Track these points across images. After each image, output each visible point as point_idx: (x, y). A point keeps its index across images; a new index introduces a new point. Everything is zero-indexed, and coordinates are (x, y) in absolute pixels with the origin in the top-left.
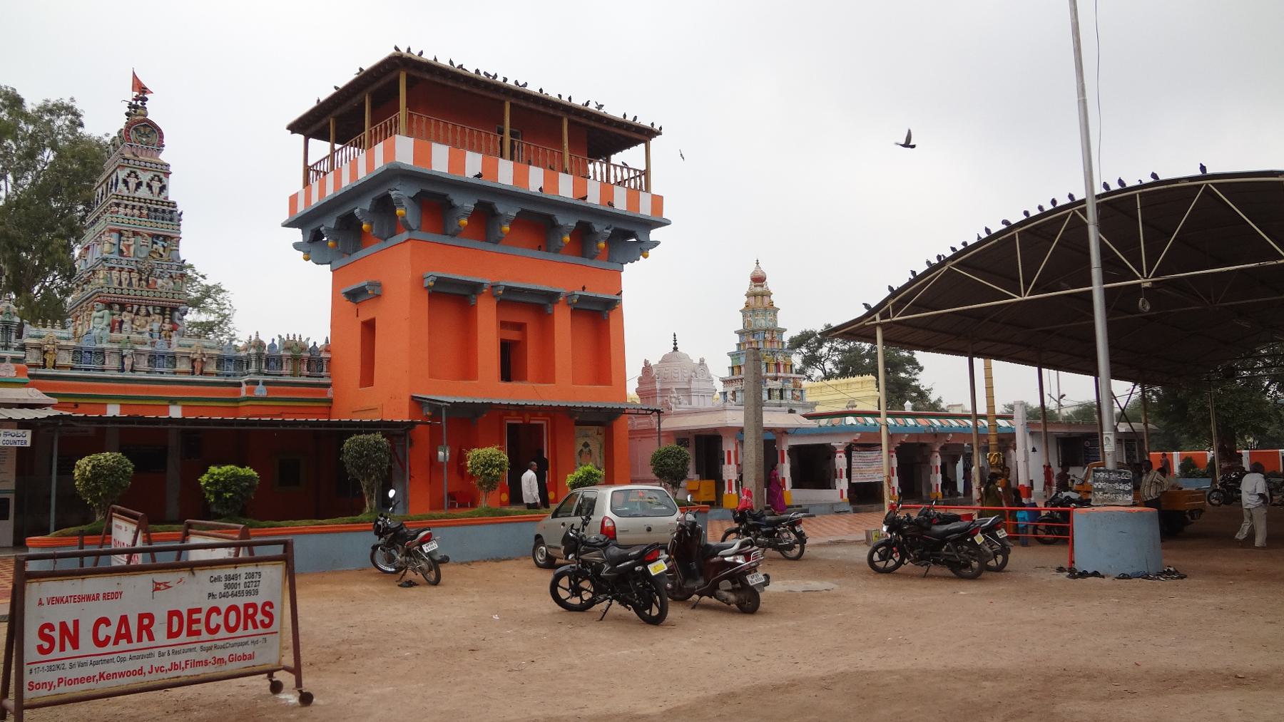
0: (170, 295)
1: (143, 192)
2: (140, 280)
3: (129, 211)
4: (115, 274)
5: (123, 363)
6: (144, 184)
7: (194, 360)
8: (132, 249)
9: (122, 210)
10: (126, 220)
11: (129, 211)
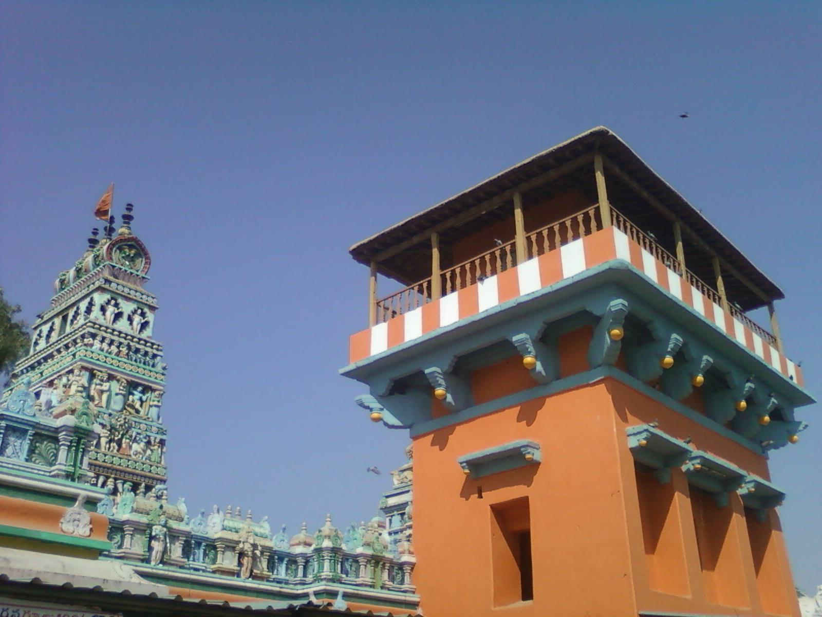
1: (122, 325)
2: (110, 441)
3: (105, 346)
5: (150, 549)
6: (125, 316)
7: (242, 555)
8: (105, 396)
9: (97, 344)
11: (105, 346)
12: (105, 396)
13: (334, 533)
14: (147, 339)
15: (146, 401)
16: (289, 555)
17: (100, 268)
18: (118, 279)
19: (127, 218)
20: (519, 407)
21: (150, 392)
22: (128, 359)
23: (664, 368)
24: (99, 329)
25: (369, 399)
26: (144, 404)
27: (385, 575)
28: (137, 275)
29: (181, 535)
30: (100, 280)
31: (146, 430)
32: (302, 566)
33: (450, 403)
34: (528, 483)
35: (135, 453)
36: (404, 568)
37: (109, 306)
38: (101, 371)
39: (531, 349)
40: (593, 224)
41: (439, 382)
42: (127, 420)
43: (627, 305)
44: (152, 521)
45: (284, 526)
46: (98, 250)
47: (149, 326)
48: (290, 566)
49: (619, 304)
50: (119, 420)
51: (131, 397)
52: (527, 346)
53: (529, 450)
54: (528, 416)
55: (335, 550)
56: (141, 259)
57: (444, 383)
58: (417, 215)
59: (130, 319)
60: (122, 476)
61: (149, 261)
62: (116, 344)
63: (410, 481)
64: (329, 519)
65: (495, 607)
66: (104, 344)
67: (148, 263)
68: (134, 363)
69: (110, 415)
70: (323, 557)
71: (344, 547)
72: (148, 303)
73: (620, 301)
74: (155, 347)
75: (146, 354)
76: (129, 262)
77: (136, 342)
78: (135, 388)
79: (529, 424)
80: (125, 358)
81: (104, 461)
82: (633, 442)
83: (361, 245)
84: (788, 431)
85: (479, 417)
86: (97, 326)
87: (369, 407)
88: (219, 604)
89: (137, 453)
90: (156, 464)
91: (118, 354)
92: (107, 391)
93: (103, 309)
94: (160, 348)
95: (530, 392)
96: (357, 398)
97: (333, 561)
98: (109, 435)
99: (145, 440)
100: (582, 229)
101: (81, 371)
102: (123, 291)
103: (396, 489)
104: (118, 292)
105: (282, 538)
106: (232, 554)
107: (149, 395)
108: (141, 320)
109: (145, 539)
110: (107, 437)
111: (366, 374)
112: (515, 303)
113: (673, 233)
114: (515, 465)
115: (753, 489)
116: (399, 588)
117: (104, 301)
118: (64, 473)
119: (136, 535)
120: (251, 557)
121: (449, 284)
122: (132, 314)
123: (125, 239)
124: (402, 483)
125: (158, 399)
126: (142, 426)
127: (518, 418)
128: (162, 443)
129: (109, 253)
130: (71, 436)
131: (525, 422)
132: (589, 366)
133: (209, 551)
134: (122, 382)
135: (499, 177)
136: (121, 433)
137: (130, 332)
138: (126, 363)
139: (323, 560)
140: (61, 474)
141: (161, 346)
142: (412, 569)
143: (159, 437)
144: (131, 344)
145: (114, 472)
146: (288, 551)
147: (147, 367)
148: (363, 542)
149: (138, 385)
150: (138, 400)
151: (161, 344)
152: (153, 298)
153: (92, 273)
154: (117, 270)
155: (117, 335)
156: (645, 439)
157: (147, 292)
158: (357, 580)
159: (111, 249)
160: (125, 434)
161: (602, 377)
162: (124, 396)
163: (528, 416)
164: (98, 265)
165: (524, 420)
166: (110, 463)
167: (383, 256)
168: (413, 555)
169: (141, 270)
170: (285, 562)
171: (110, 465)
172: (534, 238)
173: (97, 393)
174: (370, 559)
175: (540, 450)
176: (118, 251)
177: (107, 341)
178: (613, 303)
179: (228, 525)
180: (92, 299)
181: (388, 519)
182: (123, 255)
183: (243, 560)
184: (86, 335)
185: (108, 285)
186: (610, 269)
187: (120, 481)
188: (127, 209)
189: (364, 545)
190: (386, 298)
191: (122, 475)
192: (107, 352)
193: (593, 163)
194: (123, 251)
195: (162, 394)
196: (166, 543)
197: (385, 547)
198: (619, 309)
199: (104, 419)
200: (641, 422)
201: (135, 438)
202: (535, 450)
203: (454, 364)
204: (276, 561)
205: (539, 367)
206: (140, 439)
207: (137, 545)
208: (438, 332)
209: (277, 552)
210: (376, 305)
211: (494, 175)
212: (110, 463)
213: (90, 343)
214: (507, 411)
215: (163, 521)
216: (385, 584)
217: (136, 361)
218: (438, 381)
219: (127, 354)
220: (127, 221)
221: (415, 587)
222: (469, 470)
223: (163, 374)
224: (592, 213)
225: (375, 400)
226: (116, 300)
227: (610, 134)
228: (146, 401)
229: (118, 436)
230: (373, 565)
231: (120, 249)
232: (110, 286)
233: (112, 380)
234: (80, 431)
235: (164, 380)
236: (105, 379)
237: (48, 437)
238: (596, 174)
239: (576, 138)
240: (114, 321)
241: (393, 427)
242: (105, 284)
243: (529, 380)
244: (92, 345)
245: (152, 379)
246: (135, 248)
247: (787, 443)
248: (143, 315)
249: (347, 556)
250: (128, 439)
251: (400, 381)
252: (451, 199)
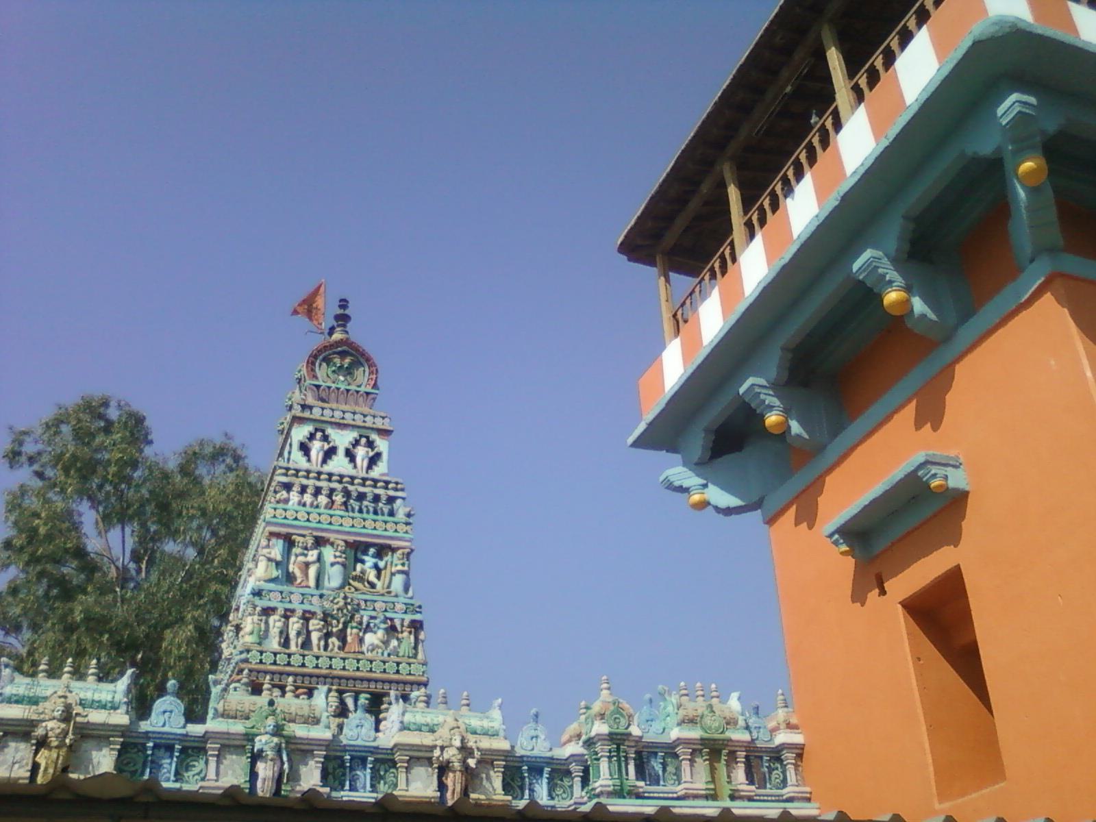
0: (390, 667)
1: (339, 464)
2: (328, 635)
3: (308, 498)
4: (275, 622)
7: (444, 769)
8: (312, 571)
10: (302, 515)
11: (308, 498)
12: (312, 571)
13: (612, 708)
15: (385, 568)
16: (550, 761)
18: (328, 402)
21: (390, 553)
22: (347, 510)
25: (680, 473)
26: (383, 572)
27: (740, 774)
29: (315, 748)
31: (386, 611)
32: (579, 779)
34: (954, 538)
35: (370, 648)
38: (304, 536)
39: (892, 274)
41: (767, 403)
42: (349, 600)
44: (253, 727)
45: (534, 711)
48: (559, 782)
49: (1014, 103)
50: (336, 601)
51: (359, 567)
52: (880, 271)
54: (931, 414)
55: (617, 740)
59: (350, 455)
60: (307, 682)
61: (374, 368)
64: (605, 685)
65: (940, 803)
66: (305, 495)
69: (321, 596)
70: (596, 753)
71: (635, 731)
74: (390, 486)
75: (377, 498)
76: (344, 376)
77: (359, 484)
78: (365, 552)
79: (935, 428)
80: (340, 510)
81: (317, 667)
87: (681, 487)
89: (373, 648)
90: (406, 659)
92: (314, 563)
93: (305, 448)
94: (399, 486)
96: (662, 478)
97: (615, 758)
98: (323, 626)
99: (383, 626)
101: (269, 540)
105: (533, 733)
106: (427, 770)
107: (388, 558)
108: (367, 452)
109: (245, 761)
110: (319, 630)
116: (778, 796)
119: (228, 757)
120: (460, 771)
122: (351, 447)
125: (401, 562)
126: (377, 605)
127: (915, 425)
128: (416, 626)
129: (309, 369)
132: (1014, 272)
133: (386, 771)
134: (338, 546)
136: (342, 620)
137: (353, 472)
138: (342, 517)
139: (598, 759)
141: (402, 484)
142: (800, 756)
143: (408, 618)
144: (350, 488)
145: (336, 681)
146: (549, 754)
147: (380, 517)
148: (680, 717)
149: (368, 546)
150: (370, 568)
151: (399, 480)
154: (324, 390)
155: (326, 480)
159: (313, 364)
160: (350, 622)
162: (344, 565)
163: (931, 414)
165: (926, 423)
166: (327, 668)
167: (670, 239)
168: (800, 731)
169: (364, 384)
170: (546, 775)
171: (327, 671)
173: (299, 568)
174: (700, 747)
176: (324, 364)
177: (310, 490)
178: (1000, 110)
179: (413, 720)
182: (334, 368)
183: (447, 779)
185: (309, 412)
187: (348, 694)
188: (341, 307)
189: (683, 722)
191: (351, 683)
192: (312, 505)
195: (409, 554)
196: (283, 763)
199: (312, 604)
201: (368, 625)
202: (950, 469)
206: (375, 625)
207: (230, 772)
209: (525, 759)
212: (327, 668)
213: (282, 498)
215: (270, 726)
216: (738, 791)
219: (345, 504)
221: (808, 789)
222: (848, 546)
223: (407, 524)
225: (690, 473)
226: (323, 431)
228: (385, 568)
229: (337, 626)
230: (708, 757)
231: (327, 360)
232: (311, 413)
233: (324, 545)
236: (309, 545)
240: (324, 461)
241: (728, 511)
244: (287, 501)
245: (390, 533)
246: (350, 356)
249: (651, 747)
250: (356, 628)
251: (713, 426)
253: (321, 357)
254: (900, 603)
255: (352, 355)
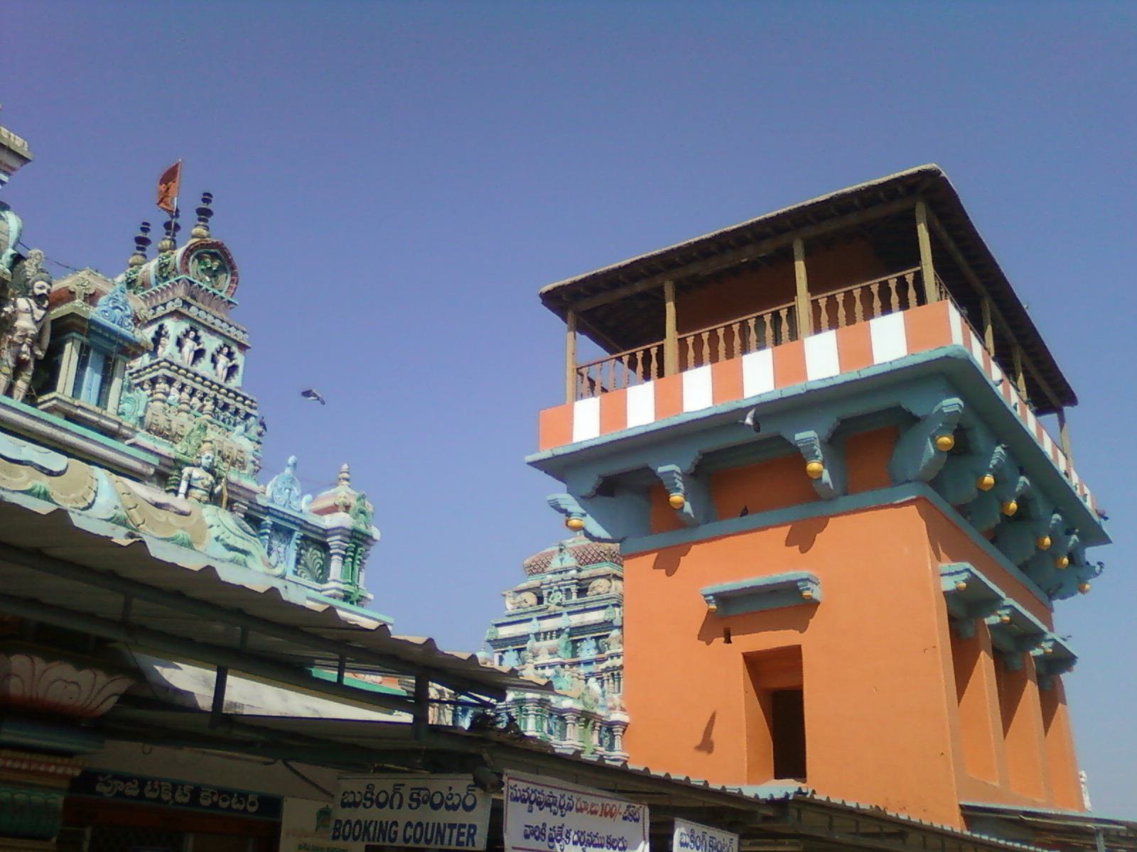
3: (185, 396)
6: (208, 356)
11: (185, 396)
14: (238, 391)
17: (170, 283)
19: (204, 214)
20: (789, 527)
23: (979, 489)
24: (176, 372)
28: (222, 298)
30: (176, 301)
33: (688, 514)
36: (614, 730)
37: (187, 340)
40: (912, 294)
41: (678, 486)
43: (963, 406)
46: (168, 257)
47: (237, 373)
52: (815, 447)
53: (809, 586)
54: (802, 538)
56: (225, 275)
57: (682, 488)
58: (649, 254)
59: (214, 360)
62: (199, 395)
63: (531, 606)
66: (183, 394)
67: (235, 281)
68: (222, 424)
70: (527, 711)
72: (238, 339)
73: (957, 400)
74: (247, 402)
75: (237, 412)
76: (210, 277)
82: (949, 584)
83: (559, 287)
84: (1078, 578)
85: (729, 536)
86: (174, 368)
88: (698, 784)
91: (200, 410)
93: (179, 343)
94: (254, 404)
95: (805, 508)
96: (550, 497)
100: (895, 299)
102: (206, 320)
103: (509, 616)
104: (199, 319)
108: (194, 345)
111: (562, 467)
112: (803, 389)
113: (981, 310)
114: (789, 602)
115: (1050, 650)
117: (182, 332)
118: (342, 594)
121: (691, 354)
122: (216, 353)
123: (207, 245)
124: (519, 608)
130: (345, 542)
131: (798, 546)
132: (893, 481)
135: (778, 215)
140: (338, 595)
141: (255, 403)
144: (219, 396)
151: (255, 399)
152: (244, 332)
153: (156, 288)
154: (196, 287)
156: (965, 581)
157: (236, 325)
158: (564, 743)
159: (188, 257)
161: (913, 497)
163: (802, 538)
164: (166, 279)
165: (796, 544)
169: (225, 291)
172: (823, 302)
175: (819, 585)
176: (196, 261)
177: (188, 390)
180: (161, 327)
181: (496, 657)
182: (203, 267)
184: (160, 380)
186: (947, 357)
188: (205, 200)
190: (602, 360)
193: (913, 210)
194: (202, 262)
195: (258, 471)
197: (596, 701)
198: (954, 411)
200: (950, 560)
202: (814, 585)
203: (697, 462)
204: (460, 713)
205: (826, 477)
208: (675, 420)
210: (575, 371)
211: (772, 212)
214: (770, 531)
217: (223, 421)
218: (676, 484)
219: (214, 411)
220: (203, 217)
221: (627, 755)
222: (717, 605)
224: (910, 278)
226: (196, 331)
227: (942, 175)
230: (583, 724)
231: (200, 258)
234: (357, 535)
235: (260, 451)
237: (315, 542)
238: (919, 227)
239: (897, 175)
242: (182, 307)
243: (809, 491)
246: (216, 257)
247: (1076, 593)
248: (230, 355)
251: (619, 480)
252: (704, 237)
253: (195, 254)
254: (743, 654)
255: (220, 259)
